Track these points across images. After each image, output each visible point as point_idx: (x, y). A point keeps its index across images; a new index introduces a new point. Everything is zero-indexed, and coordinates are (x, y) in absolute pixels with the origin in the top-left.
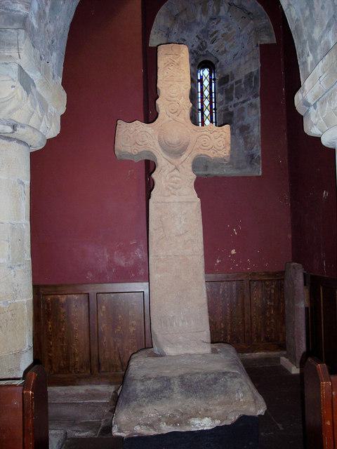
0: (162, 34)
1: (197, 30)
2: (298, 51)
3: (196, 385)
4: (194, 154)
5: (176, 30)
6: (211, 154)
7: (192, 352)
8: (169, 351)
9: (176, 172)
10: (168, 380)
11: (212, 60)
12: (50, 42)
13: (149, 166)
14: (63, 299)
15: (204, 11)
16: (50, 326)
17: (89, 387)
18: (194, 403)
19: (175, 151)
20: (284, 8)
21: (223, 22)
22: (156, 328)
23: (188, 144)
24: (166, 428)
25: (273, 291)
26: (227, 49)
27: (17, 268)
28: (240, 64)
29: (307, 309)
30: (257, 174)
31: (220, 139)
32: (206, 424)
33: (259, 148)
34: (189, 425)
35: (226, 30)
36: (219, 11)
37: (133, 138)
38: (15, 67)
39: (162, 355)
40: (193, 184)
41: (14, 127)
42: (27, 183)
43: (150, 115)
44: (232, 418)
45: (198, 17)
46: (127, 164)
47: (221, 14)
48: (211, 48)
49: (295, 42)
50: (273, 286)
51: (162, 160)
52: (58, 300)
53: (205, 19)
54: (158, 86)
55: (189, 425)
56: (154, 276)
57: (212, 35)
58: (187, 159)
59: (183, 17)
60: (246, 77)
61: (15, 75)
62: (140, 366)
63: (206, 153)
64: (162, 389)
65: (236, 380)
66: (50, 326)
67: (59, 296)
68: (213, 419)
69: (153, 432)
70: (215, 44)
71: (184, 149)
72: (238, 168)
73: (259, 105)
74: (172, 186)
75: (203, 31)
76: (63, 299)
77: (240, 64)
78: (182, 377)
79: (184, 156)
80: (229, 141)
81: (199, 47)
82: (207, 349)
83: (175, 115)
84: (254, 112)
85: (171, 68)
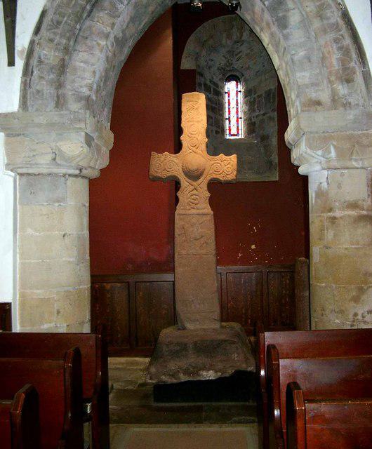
0: (192, 59)
1: (223, 51)
3: (208, 348)
4: (209, 178)
5: (204, 53)
6: (221, 178)
7: (205, 327)
8: (188, 325)
9: (195, 192)
10: (186, 345)
11: (238, 74)
12: (103, 103)
13: (177, 185)
14: (108, 286)
15: (229, 37)
16: (98, 308)
17: (128, 359)
18: (203, 360)
19: (194, 175)
21: (245, 45)
22: (179, 307)
24: (183, 378)
26: (251, 66)
27: (81, 265)
28: (261, 80)
30: (274, 179)
32: (210, 375)
33: (277, 156)
34: (199, 375)
35: (248, 51)
36: (242, 36)
37: (165, 164)
38: (83, 134)
39: (184, 328)
40: (207, 201)
41: (81, 170)
42: (87, 205)
43: (178, 147)
44: (230, 372)
45: (224, 41)
46: (157, 180)
47: (243, 38)
48: (237, 65)
51: (185, 182)
52: (104, 287)
53: (229, 42)
54: (182, 125)
55: (199, 375)
56: (179, 270)
57: (236, 55)
58: (203, 183)
59: (211, 42)
60: (266, 92)
61: (83, 139)
62: (167, 334)
63: (218, 177)
64: (180, 350)
65: (233, 346)
66: (98, 308)
67: (105, 284)
68: (216, 372)
69: (174, 381)
70: (240, 61)
71: (201, 174)
72: (259, 173)
73: (276, 119)
75: (229, 52)
76: (108, 286)
77: (261, 80)
78: (195, 343)
80: (236, 167)
81: (226, 64)
82: (217, 325)
84: (272, 124)
85: (192, 112)
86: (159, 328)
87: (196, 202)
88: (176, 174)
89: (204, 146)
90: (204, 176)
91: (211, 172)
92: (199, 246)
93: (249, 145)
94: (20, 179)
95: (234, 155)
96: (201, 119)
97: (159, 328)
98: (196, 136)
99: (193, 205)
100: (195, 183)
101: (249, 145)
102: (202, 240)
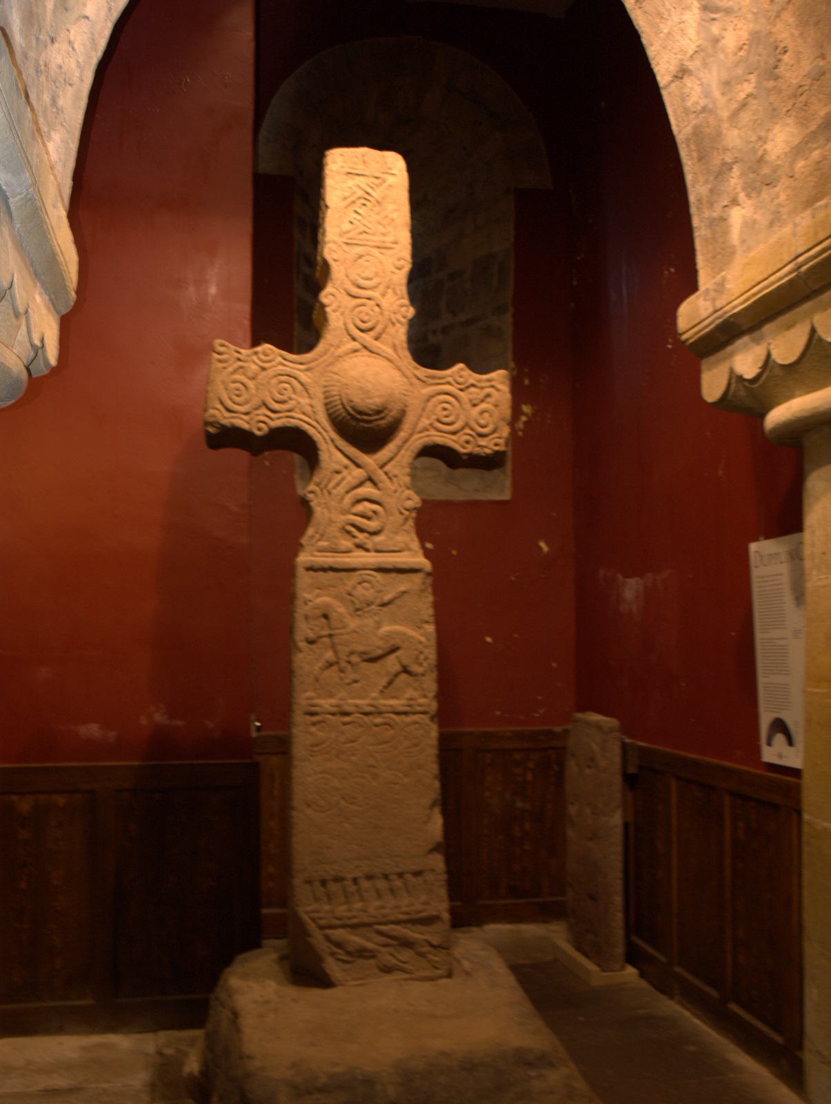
2: (696, 188)
9: (368, 490)
19: (366, 429)
20: (663, 78)
23: (403, 413)
25: (530, 777)
29: (626, 826)
31: (483, 406)
40: (411, 523)
49: (689, 178)
50: (531, 765)
67: (15, 798)
74: (353, 525)
79: (390, 448)
83: (368, 338)
86: (715, 29)
87: (373, 525)
88: (297, 420)
89: (400, 333)
90: (402, 435)
91: (425, 422)
92: (384, 682)
93: (753, 195)
94: (382, 343)
95: (502, 372)
96: (389, 239)
97: (715, 29)
98: (375, 294)
99: (361, 537)
100: (368, 460)
101: (753, 195)
102: (392, 663)
